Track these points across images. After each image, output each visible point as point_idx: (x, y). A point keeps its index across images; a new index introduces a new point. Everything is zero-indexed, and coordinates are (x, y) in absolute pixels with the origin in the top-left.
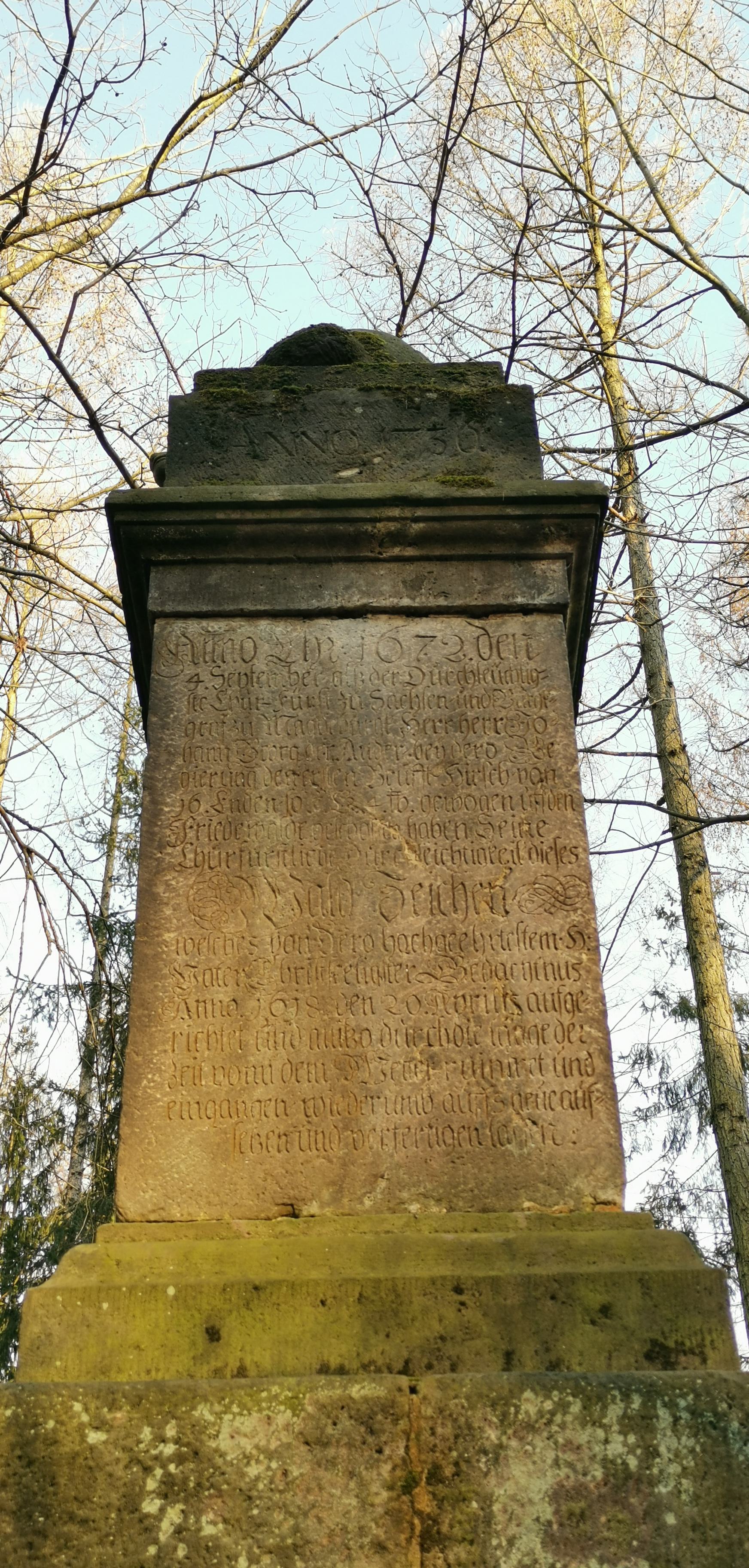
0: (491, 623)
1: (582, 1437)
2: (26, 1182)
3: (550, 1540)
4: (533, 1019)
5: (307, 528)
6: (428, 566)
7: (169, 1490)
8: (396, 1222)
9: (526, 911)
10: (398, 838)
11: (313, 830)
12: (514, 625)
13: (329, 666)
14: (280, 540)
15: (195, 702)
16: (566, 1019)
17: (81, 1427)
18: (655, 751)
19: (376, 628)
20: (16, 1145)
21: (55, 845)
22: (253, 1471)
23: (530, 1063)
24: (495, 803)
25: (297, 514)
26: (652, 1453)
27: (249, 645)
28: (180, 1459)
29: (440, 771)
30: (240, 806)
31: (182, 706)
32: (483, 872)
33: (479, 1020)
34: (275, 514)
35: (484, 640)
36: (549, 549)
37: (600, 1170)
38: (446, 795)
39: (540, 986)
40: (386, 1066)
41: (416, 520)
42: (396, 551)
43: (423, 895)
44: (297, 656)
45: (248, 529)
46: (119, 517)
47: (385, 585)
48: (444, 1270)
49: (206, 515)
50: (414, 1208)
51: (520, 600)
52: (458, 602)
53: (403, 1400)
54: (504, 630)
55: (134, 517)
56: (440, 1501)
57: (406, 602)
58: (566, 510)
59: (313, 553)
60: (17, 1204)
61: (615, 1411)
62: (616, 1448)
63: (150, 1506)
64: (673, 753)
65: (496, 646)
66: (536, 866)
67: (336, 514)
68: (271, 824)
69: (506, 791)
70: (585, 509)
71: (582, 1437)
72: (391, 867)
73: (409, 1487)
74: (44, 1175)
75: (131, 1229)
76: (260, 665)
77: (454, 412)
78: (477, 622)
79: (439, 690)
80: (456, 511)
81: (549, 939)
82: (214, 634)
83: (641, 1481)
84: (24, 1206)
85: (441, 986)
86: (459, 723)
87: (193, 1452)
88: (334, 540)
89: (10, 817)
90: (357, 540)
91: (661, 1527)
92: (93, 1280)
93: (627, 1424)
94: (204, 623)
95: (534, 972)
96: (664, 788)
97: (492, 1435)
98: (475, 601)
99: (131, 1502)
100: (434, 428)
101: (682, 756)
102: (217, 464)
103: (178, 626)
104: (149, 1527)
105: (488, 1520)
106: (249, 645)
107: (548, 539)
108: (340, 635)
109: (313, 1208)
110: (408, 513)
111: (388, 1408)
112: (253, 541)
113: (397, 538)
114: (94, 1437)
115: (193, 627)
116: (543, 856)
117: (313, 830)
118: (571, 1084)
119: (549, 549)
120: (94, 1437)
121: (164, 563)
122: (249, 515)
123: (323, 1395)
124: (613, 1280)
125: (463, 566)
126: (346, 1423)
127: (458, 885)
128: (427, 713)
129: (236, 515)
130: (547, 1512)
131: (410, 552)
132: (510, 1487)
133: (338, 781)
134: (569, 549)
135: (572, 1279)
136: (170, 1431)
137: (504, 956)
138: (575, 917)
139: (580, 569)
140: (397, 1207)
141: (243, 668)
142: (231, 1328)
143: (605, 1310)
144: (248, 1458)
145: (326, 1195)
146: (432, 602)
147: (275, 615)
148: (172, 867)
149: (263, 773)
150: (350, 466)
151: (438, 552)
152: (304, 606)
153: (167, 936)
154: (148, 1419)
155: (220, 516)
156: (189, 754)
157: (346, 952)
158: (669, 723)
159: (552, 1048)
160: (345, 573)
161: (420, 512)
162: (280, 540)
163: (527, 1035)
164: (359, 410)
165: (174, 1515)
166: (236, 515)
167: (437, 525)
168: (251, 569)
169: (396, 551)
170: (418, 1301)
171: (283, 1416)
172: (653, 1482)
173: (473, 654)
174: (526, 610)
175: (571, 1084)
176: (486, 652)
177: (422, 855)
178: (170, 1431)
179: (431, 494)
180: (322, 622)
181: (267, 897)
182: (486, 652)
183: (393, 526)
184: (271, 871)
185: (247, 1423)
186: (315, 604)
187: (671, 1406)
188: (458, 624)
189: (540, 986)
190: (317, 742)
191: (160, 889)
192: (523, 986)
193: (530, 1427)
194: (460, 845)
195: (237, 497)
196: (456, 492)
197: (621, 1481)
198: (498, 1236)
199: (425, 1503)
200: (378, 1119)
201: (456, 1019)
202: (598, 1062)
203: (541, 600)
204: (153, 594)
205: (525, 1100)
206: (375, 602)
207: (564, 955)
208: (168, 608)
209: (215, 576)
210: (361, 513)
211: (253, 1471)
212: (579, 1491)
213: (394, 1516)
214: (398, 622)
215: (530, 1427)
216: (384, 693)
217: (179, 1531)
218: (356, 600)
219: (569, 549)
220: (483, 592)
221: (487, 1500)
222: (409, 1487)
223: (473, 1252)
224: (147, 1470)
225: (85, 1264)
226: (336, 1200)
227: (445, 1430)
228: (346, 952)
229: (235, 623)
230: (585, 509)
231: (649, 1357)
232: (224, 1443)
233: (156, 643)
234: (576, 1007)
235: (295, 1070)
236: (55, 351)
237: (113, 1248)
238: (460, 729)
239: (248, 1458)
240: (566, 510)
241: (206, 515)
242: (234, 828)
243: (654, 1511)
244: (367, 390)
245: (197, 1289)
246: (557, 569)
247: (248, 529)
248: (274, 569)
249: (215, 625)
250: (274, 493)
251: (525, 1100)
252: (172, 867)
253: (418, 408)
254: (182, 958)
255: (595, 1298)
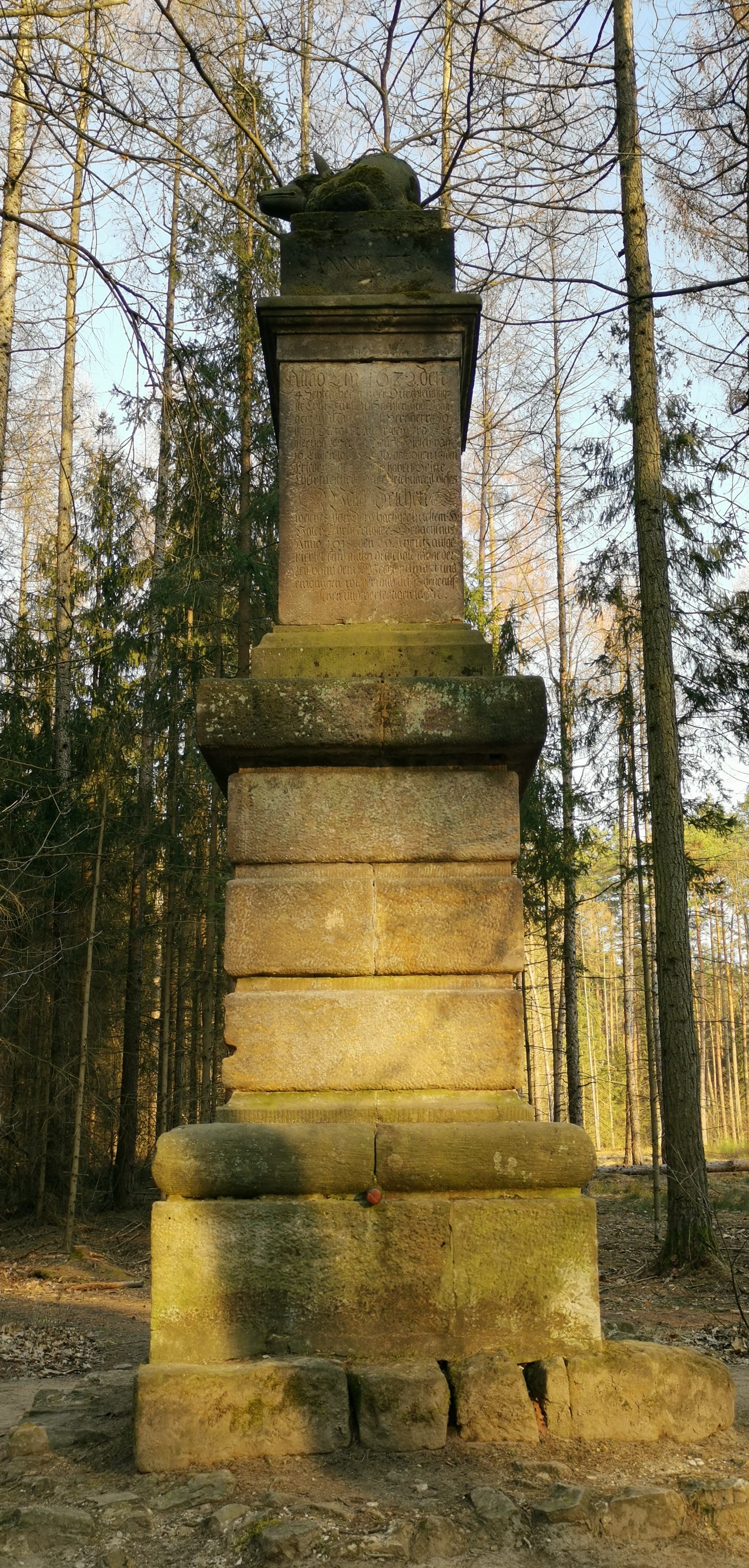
0: (428, 365)
1: (435, 696)
2: (115, 539)
3: (423, 724)
4: (434, 550)
5: (347, 319)
6: (403, 337)
7: (306, 710)
8: (380, 626)
9: (435, 505)
10: (384, 471)
11: (350, 468)
12: (436, 367)
13: (356, 388)
14: (334, 324)
15: (299, 406)
16: (447, 550)
17: (278, 692)
18: (620, 209)
19: (377, 368)
20: (104, 511)
21: (152, 307)
22: (332, 705)
23: (432, 567)
24: (425, 455)
25: (342, 312)
26: (456, 700)
27: (321, 377)
28: (309, 701)
29: (402, 440)
30: (319, 456)
31: (293, 407)
32: (418, 487)
33: (413, 550)
34: (332, 312)
35: (424, 375)
36: (455, 329)
37: (455, 608)
38: (404, 452)
39: (438, 536)
40: (377, 568)
41: (395, 315)
42: (386, 329)
43: (393, 497)
44: (342, 383)
45: (320, 319)
46: (263, 313)
47: (379, 346)
48: (396, 644)
49: (301, 312)
50: (386, 621)
51: (440, 355)
52: (413, 356)
53: (379, 685)
54: (433, 370)
55: (269, 313)
56: (390, 714)
57: (390, 356)
58: (463, 311)
59: (349, 330)
60: (110, 556)
61: (446, 689)
62: (446, 699)
63: (301, 714)
64: (634, 212)
65: (428, 379)
66: (439, 484)
67: (359, 312)
68: (332, 464)
69: (429, 450)
70: (471, 310)
71: (435, 696)
72: (381, 485)
73: (380, 709)
74: (128, 534)
75: (285, 628)
76: (326, 387)
77: (416, 245)
78: (421, 366)
79: (403, 400)
80: (413, 311)
81: (442, 516)
82: (306, 371)
83: (452, 709)
84: (115, 558)
85: (399, 536)
86: (411, 417)
87: (313, 699)
88: (358, 324)
89: (121, 290)
90: (370, 324)
91: (457, 721)
92: (274, 646)
93: (449, 692)
94: (302, 365)
95: (436, 531)
96: (624, 242)
97: (407, 695)
98: (421, 356)
99: (295, 713)
100: (405, 255)
101: (642, 214)
102: (304, 276)
103: (291, 366)
104: (300, 720)
105: (404, 719)
106: (321, 377)
107: (454, 324)
108: (361, 372)
109: (350, 621)
110: (391, 311)
111: (374, 687)
112: (323, 325)
113: (387, 324)
114: (282, 694)
115: (297, 367)
116: (443, 480)
117: (350, 468)
118: (447, 575)
119: (455, 329)
120: (282, 694)
121: (283, 334)
122: (320, 313)
123: (354, 683)
124: (453, 648)
125: (416, 336)
126: (361, 691)
127: (407, 493)
128: (398, 412)
129: (314, 313)
130: (423, 717)
131: (392, 330)
132: (412, 710)
133: (360, 445)
134: (463, 329)
135: (439, 647)
136: (306, 693)
137: (425, 523)
138: (453, 507)
139: (469, 335)
140: (380, 621)
141: (319, 389)
142: (322, 661)
143: (450, 657)
144: (330, 701)
145: (355, 616)
146: (402, 356)
147: (332, 361)
148: (293, 484)
149: (328, 441)
150: (365, 277)
151: (405, 330)
152: (345, 358)
153: (293, 514)
154: (298, 689)
155: (308, 313)
156: (297, 431)
157: (363, 522)
158: (633, 184)
159: (440, 561)
160: (363, 340)
161: (397, 312)
162: (334, 324)
163: (431, 556)
164: (370, 244)
165: (308, 717)
166: (314, 313)
167: (404, 318)
168: (321, 338)
169: (386, 329)
170: (386, 654)
171: (341, 689)
172: (456, 709)
173: (419, 383)
174: (443, 360)
175: (447, 575)
176: (424, 381)
177: (394, 479)
178: (306, 693)
179: (402, 303)
180: (353, 365)
181: (331, 498)
182: (424, 381)
183: (385, 318)
184: (332, 486)
185: (330, 691)
186: (350, 357)
187: (464, 687)
188: (412, 365)
189: (438, 536)
190: (351, 426)
191: (288, 494)
192: (431, 536)
193: (419, 693)
194: (409, 475)
195: (315, 304)
196: (413, 302)
197: (446, 708)
198: (415, 632)
199: (385, 714)
200: (375, 588)
201: (405, 549)
202: (458, 567)
203: (450, 355)
204: (279, 351)
205: (429, 581)
206: (376, 356)
207: (448, 524)
208: (286, 358)
209: (306, 341)
210: (371, 312)
211: (332, 705)
212: (433, 711)
213: (375, 718)
214: (387, 365)
215: (419, 693)
216: (380, 402)
217: (310, 721)
218: (368, 355)
219: (463, 329)
220: (425, 351)
221: (404, 714)
222: (380, 709)
223: (405, 638)
224: (299, 704)
225: (271, 640)
226: (358, 618)
227: (393, 694)
228: (363, 522)
229: (315, 365)
230: (471, 310)
231: (463, 673)
232: (323, 696)
233: (281, 376)
234: (451, 545)
235: (343, 569)
236: (165, 6)
237: (280, 634)
238: (411, 420)
239: (330, 701)
240: (463, 311)
241: (301, 312)
242: (317, 467)
243: (455, 717)
244: (373, 231)
245: (310, 649)
246: (457, 338)
247: (320, 319)
248: (332, 337)
249: (307, 367)
250: (330, 300)
251: (429, 581)
252: (293, 484)
253: (398, 243)
254: (298, 523)
255: (446, 653)
